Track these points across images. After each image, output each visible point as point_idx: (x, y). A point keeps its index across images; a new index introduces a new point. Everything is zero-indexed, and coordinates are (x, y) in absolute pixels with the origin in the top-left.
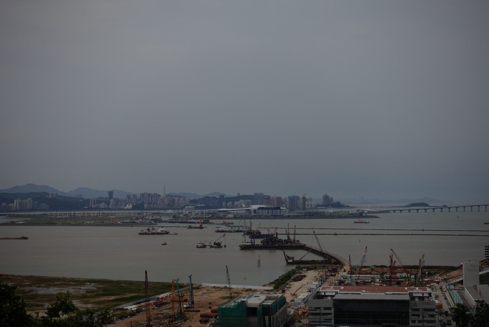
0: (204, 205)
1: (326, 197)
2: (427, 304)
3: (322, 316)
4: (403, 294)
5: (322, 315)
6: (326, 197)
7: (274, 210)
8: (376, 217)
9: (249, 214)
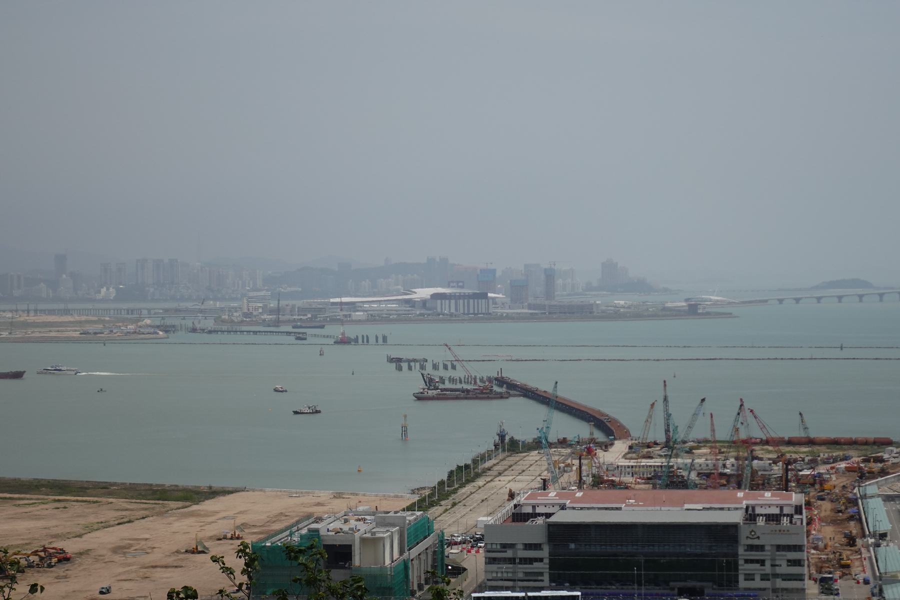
0: (300, 289)
1: (609, 268)
3: (520, 566)
4: (729, 509)
5: (520, 563)
6: (609, 268)
7: (471, 301)
9: (409, 311)
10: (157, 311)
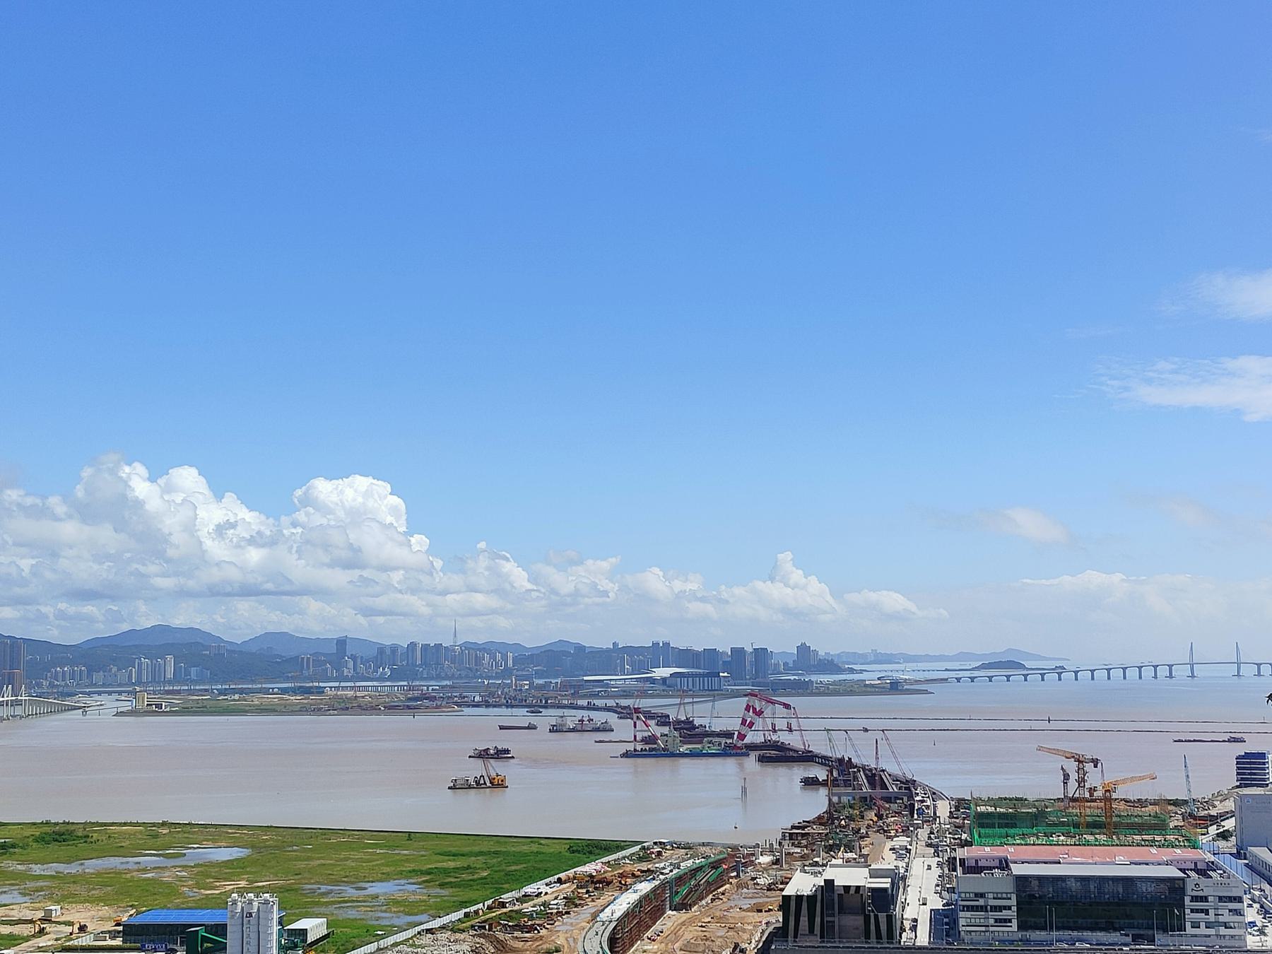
1: (803, 649)
2: (1227, 885)
7: (706, 679)
8: (925, 692)
10: (435, 687)
